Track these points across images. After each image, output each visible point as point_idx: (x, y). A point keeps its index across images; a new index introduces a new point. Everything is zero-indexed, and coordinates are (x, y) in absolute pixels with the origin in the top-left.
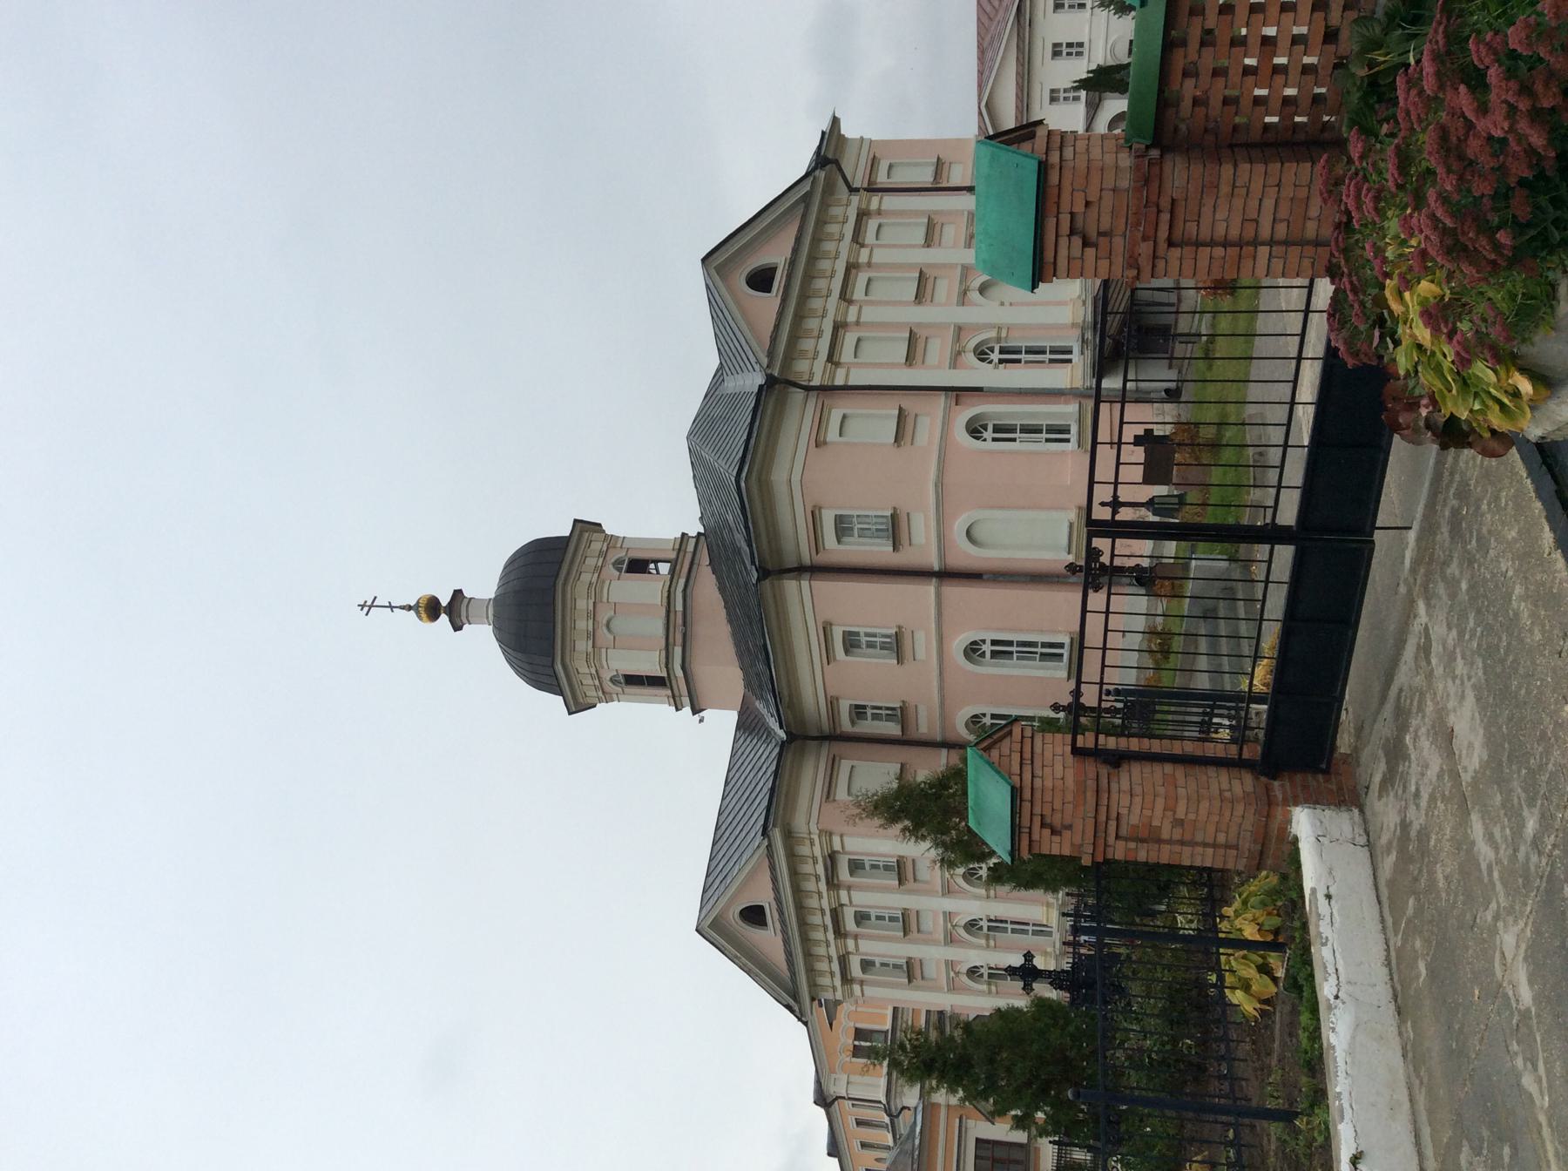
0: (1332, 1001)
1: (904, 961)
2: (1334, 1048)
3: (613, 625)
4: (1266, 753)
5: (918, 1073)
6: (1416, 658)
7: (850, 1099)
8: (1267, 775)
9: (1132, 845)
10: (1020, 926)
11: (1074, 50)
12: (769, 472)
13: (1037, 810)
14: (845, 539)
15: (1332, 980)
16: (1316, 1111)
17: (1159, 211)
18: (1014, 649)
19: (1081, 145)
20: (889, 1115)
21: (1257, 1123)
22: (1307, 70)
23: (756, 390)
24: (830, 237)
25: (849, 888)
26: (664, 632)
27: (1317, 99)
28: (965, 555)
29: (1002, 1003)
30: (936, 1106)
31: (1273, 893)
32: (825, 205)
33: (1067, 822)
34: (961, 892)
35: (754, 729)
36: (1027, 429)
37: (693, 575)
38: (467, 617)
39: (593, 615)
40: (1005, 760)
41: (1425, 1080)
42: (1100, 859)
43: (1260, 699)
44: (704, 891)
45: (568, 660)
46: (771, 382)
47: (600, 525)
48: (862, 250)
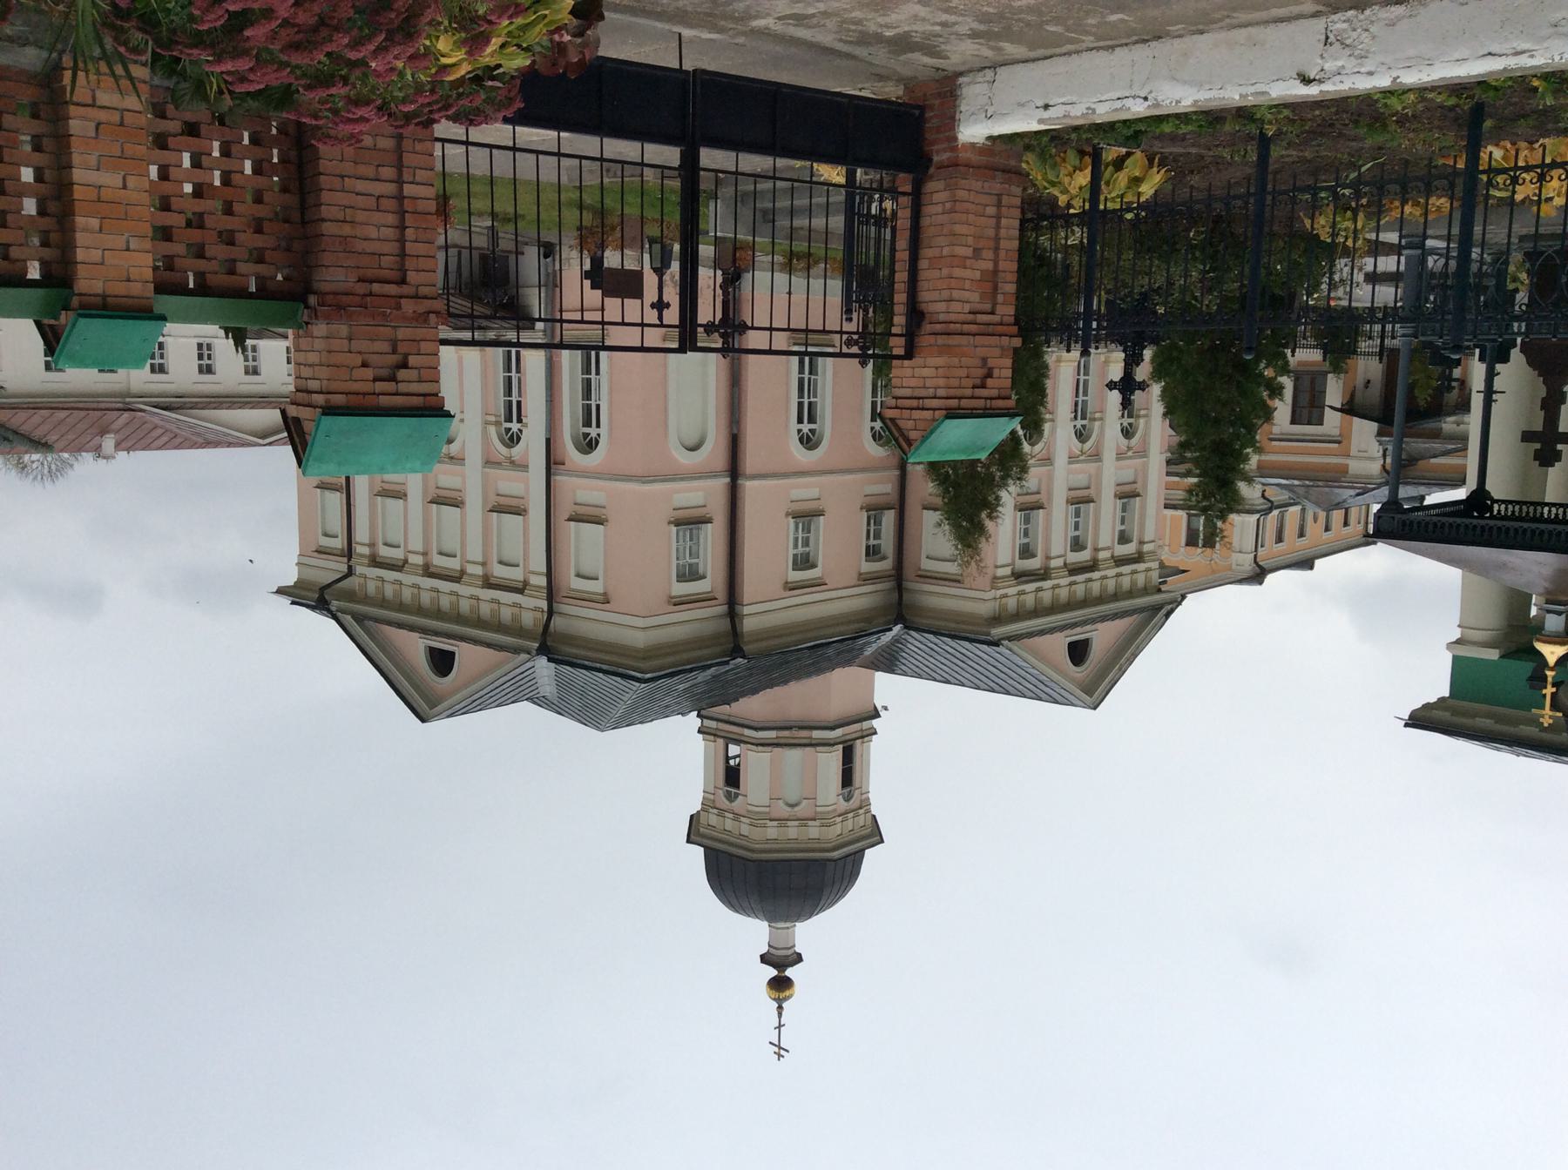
0: (1149, 103)
1: (1118, 501)
2: (1196, 101)
3: (792, 801)
4: (907, 169)
5: (1230, 494)
6: (810, 27)
7: (1256, 550)
8: (928, 168)
9: (1000, 298)
10: (1080, 388)
11: (206, 353)
12: (637, 650)
13: (968, 392)
14: (701, 571)
15: (1129, 103)
16: (1258, 116)
17: (371, 294)
18: (806, 401)
19: (306, 372)
20: (1270, 510)
21: (1271, 168)
22: (226, 153)
23: (553, 665)
24: (398, 594)
25: (1048, 558)
26: (799, 748)
27: (255, 141)
28: (714, 451)
29: (1158, 408)
30: (1260, 466)
31: (1043, 156)
32: (366, 600)
33: (978, 362)
34: (1048, 449)
35: (893, 656)
36: (587, 393)
37: (741, 721)
38: (789, 948)
39: (782, 821)
40: (921, 425)
41: (1226, 13)
42: (1015, 329)
43: (851, 176)
44: (1056, 702)
46: (545, 650)
47: (692, 816)
48: (410, 561)
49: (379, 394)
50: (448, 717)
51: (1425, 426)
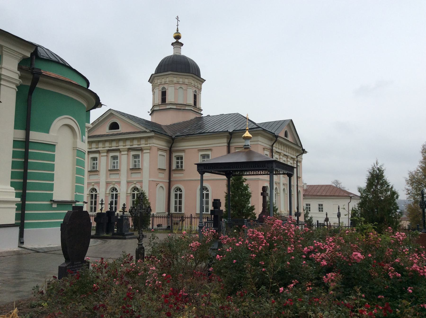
3: (181, 89)
26: (179, 104)
38: (175, 47)
39: (184, 84)
45: (171, 75)
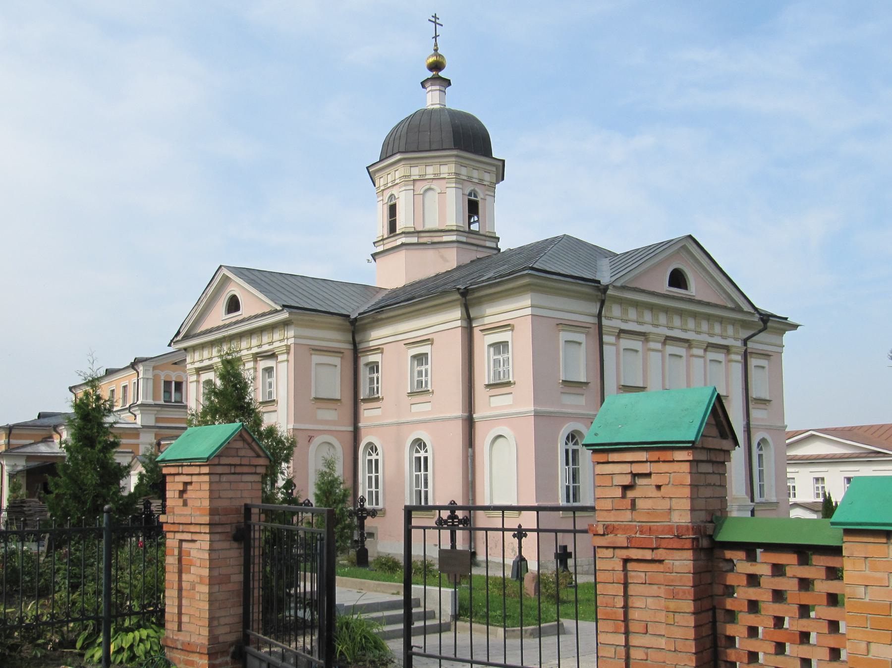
13: (195, 479)
19: (715, 479)
20: (130, 407)
32: (733, 322)
33: (189, 502)
49: (646, 462)
50: (672, 240)
51: (38, 463)
